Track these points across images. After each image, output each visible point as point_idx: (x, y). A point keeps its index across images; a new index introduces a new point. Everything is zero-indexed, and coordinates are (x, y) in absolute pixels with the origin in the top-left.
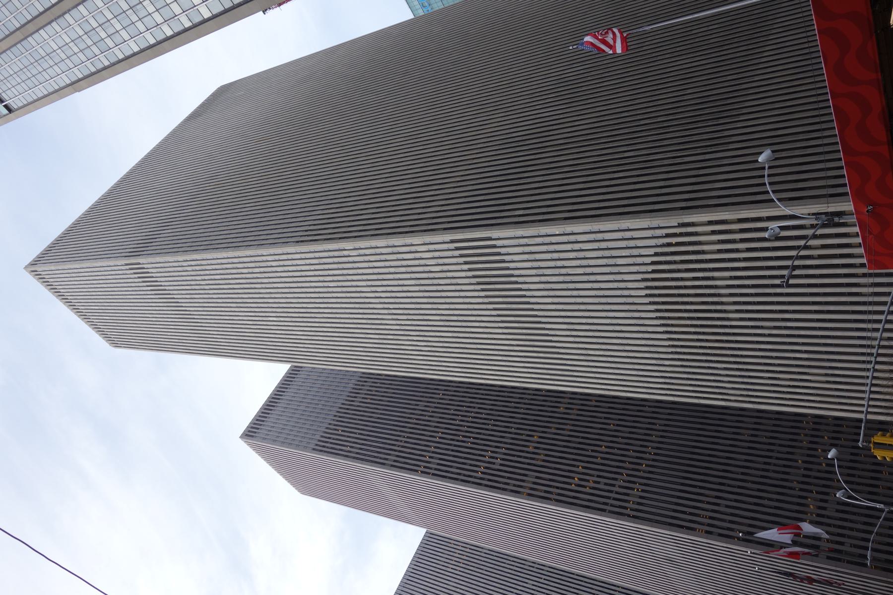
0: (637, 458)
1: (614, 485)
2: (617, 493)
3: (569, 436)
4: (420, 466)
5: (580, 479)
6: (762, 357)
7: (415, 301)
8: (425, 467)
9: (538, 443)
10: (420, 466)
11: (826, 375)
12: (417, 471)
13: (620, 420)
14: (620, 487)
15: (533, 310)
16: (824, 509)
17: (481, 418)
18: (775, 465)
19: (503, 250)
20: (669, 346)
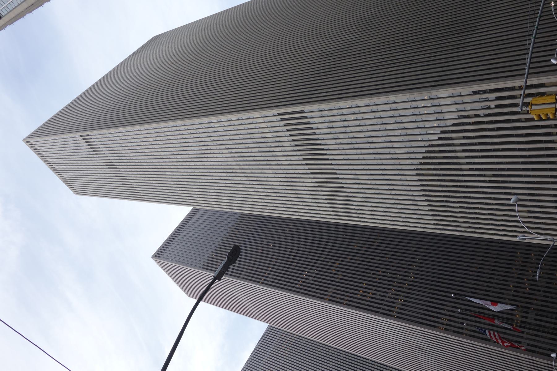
0: (402, 279)
1: (385, 296)
2: (387, 301)
3: (359, 264)
4: (261, 279)
5: (363, 292)
6: (485, 198)
7: (258, 162)
8: (264, 280)
9: (338, 267)
10: (261, 279)
11: (529, 212)
12: (259, 282)
13: (392, 255)
14: (389, 297)
15: (348, 196)
16: (526, 318)
17: (303, 251)
18: (494, 288)
19: (331, 157)
20: (434, 224)
